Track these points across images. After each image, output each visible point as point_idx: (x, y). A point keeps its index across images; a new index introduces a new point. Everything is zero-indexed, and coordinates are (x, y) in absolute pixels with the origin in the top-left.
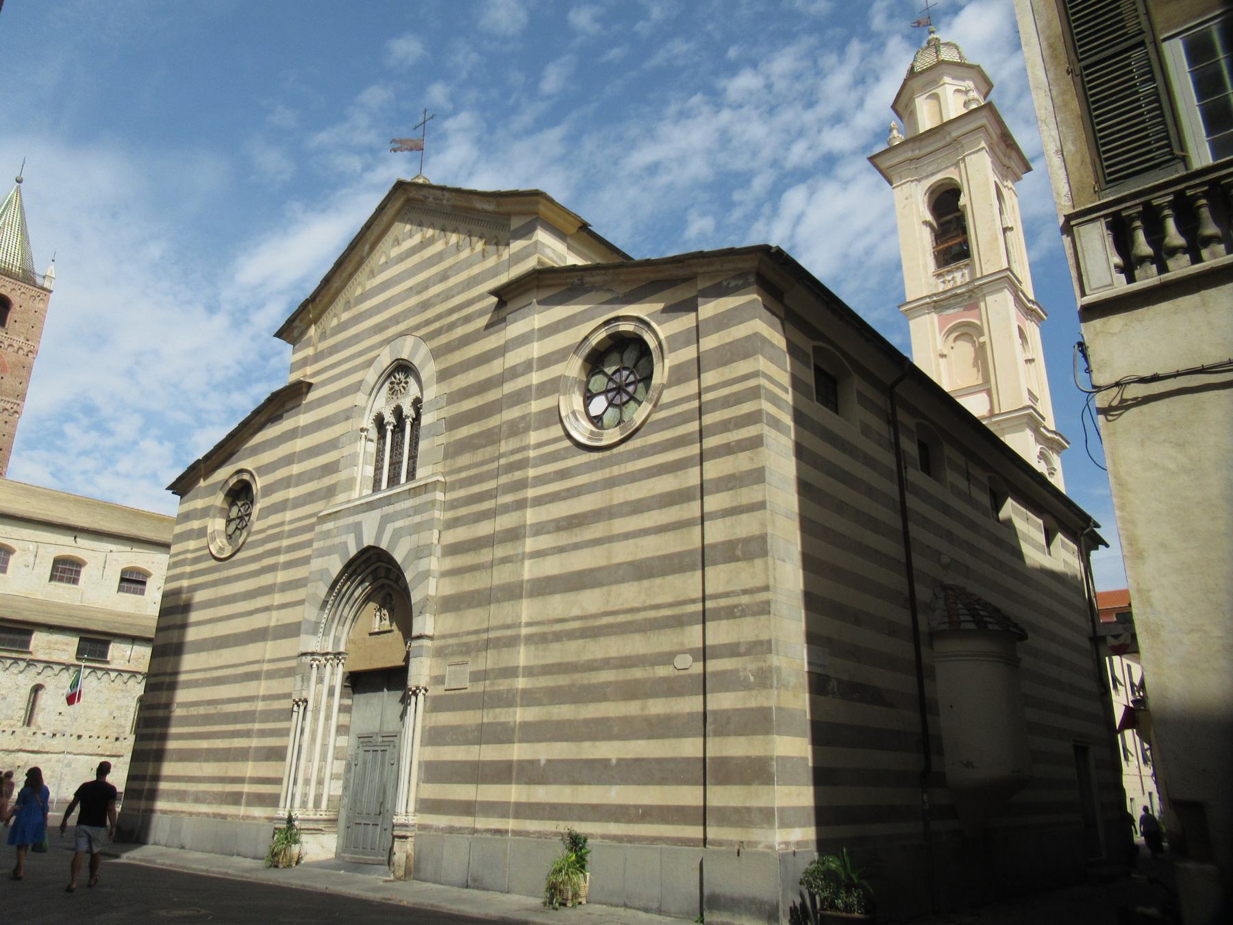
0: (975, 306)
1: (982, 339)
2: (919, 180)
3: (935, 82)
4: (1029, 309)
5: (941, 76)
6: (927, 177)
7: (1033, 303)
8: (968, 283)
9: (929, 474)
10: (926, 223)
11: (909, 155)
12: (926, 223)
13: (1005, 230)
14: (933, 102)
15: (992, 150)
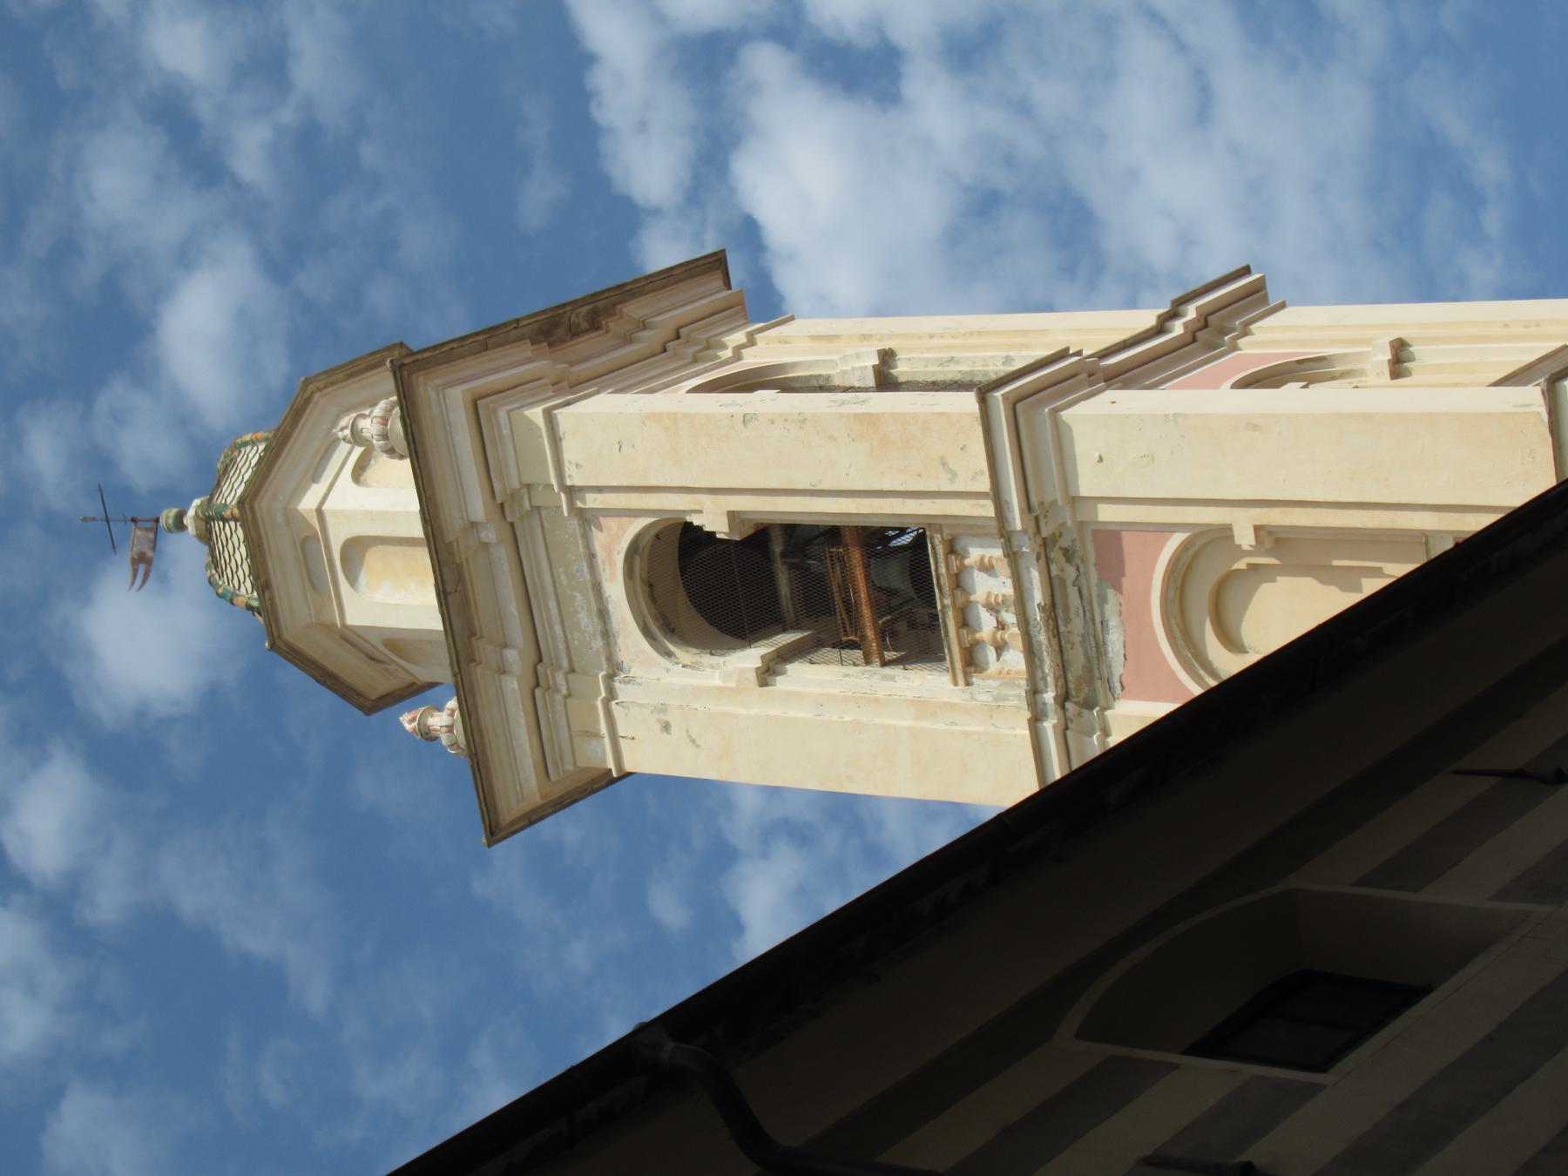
0: (1110, 540)
1: (1245, 538)
2: (615, 669)
3: (309, 541)
4: (1192, 337)
5: (292, 517)
6: (607, 635)
7: (1173, 315)
8: (1013, 556)
9: (1411, 994)
10: (768, 673)
11: (513, 687)
12: (768, 673)
13: (885, 380)
14: (373, 557)
15: (576, 386)
